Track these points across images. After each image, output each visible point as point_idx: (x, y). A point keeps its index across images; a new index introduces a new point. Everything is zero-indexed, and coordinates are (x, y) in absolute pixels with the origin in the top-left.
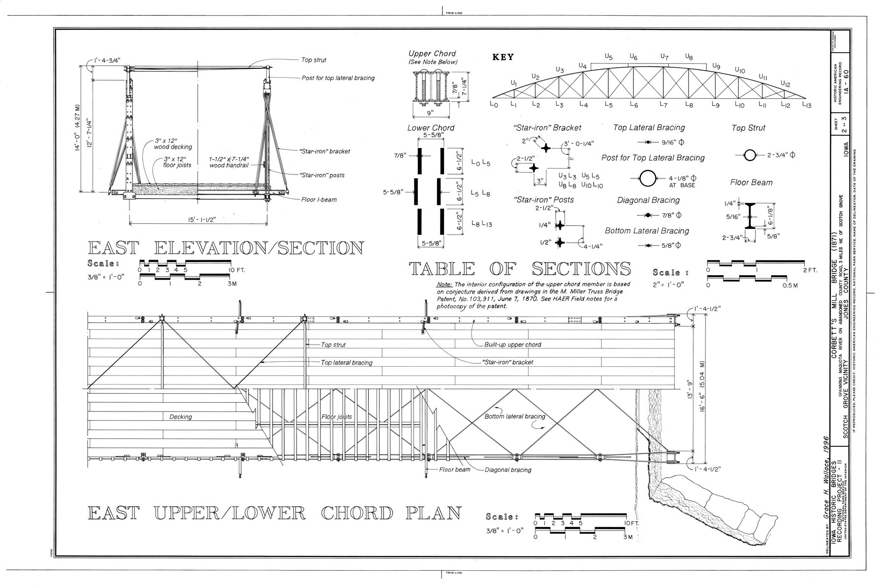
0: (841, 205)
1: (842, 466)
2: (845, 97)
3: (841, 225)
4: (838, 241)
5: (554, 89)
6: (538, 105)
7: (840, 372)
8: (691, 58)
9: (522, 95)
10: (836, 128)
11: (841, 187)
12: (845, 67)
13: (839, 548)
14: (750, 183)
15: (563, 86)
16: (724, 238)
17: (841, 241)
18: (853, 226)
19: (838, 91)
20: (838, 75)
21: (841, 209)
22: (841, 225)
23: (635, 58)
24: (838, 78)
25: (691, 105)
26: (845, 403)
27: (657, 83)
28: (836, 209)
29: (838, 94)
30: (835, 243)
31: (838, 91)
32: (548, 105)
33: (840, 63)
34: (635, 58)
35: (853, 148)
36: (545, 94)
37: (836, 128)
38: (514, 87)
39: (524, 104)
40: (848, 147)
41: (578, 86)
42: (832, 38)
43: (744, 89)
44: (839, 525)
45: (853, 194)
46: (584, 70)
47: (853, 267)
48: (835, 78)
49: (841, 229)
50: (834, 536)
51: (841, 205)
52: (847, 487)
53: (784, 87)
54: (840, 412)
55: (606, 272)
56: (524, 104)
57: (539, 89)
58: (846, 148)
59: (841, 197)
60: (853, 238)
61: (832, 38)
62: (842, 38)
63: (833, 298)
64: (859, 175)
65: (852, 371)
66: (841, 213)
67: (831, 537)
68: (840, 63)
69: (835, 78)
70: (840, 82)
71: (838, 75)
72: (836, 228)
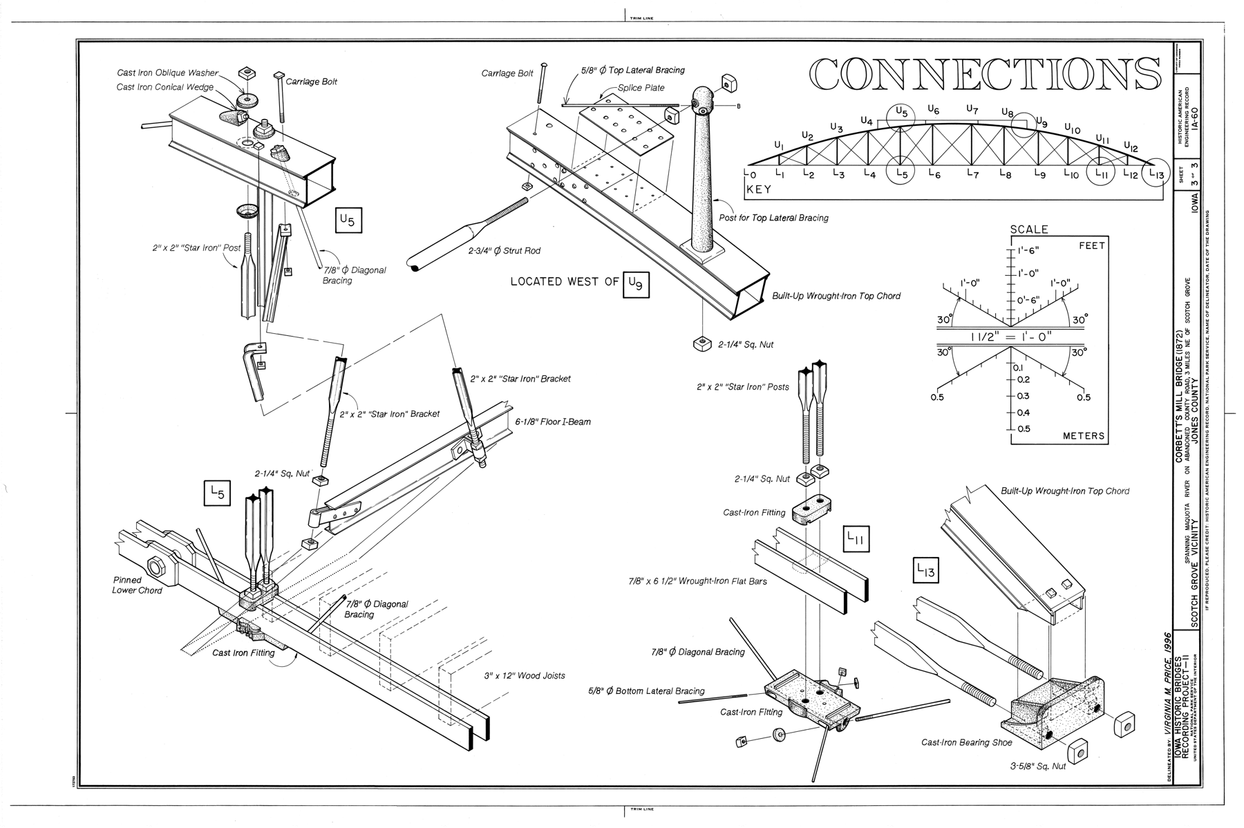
0: (1188, 293)
1: (1191, 662)
2: (1194, 135)
3: (1188, 321)
4: (1184, 344)
5: (830, 153)
6: (812, 175)
7: (1187, 528)
8: (1011, 114)
9: (789, 162)
10: (1181, 181)
11: (1188, 267)
12: (1194, 102)
13: (1186, 770)
14: (388, 415)
15: (843, 151)
16: (488, 675)
17: (1188, 344)
18: (1205, 360)
19: (1183, 127)
20: (1183, 105)
21: (1188, 299)
22: (1188, 321)
23: (937, 112)
24: (1184, 110)
25: (1009, 175)
26: (1194, 582)
27: (963, 145)
28: (1181, 299)
29: (1183, 132)
30: (1180, 347)
31: (1183, 127)
32: (824, 174)
33: (1187, 89)
34: (937, 112)
35: (1205, 209)
36: (819, 160)
37: (1181, 181)
38: (779, 151)
39: (793, 173)
40: (1198, 200)
41: (861, 150)
42: (1175, 53)
43: (1075, 153)
44: (1185, 734)
45: (1206, 273)
46: (868, 127)
47: (1205, 376)
48: (1180, 110)
49: (1188, 326)
50: (1178, 746)
51: (1188, 293)
52: (1197, 687)
53: (1128, 151)
54: (1185, 592)
55: (1098, 83)
56: (793, 173)
57: (811, 154)
58: (1195, 202)
59: (1187, 281)
60: (1205, 336)
61: (1175, 53)
62: (1189, 54)
63: (1177, 398)
64: (1214, 247)
65: (1205, 523)
66: (1187, 303)
67: (1176, 749)
68: (1187, 89)
69: (1180, 110)
70: (1188, 119)
71: (1183, 105)
72: (1180, 325)
